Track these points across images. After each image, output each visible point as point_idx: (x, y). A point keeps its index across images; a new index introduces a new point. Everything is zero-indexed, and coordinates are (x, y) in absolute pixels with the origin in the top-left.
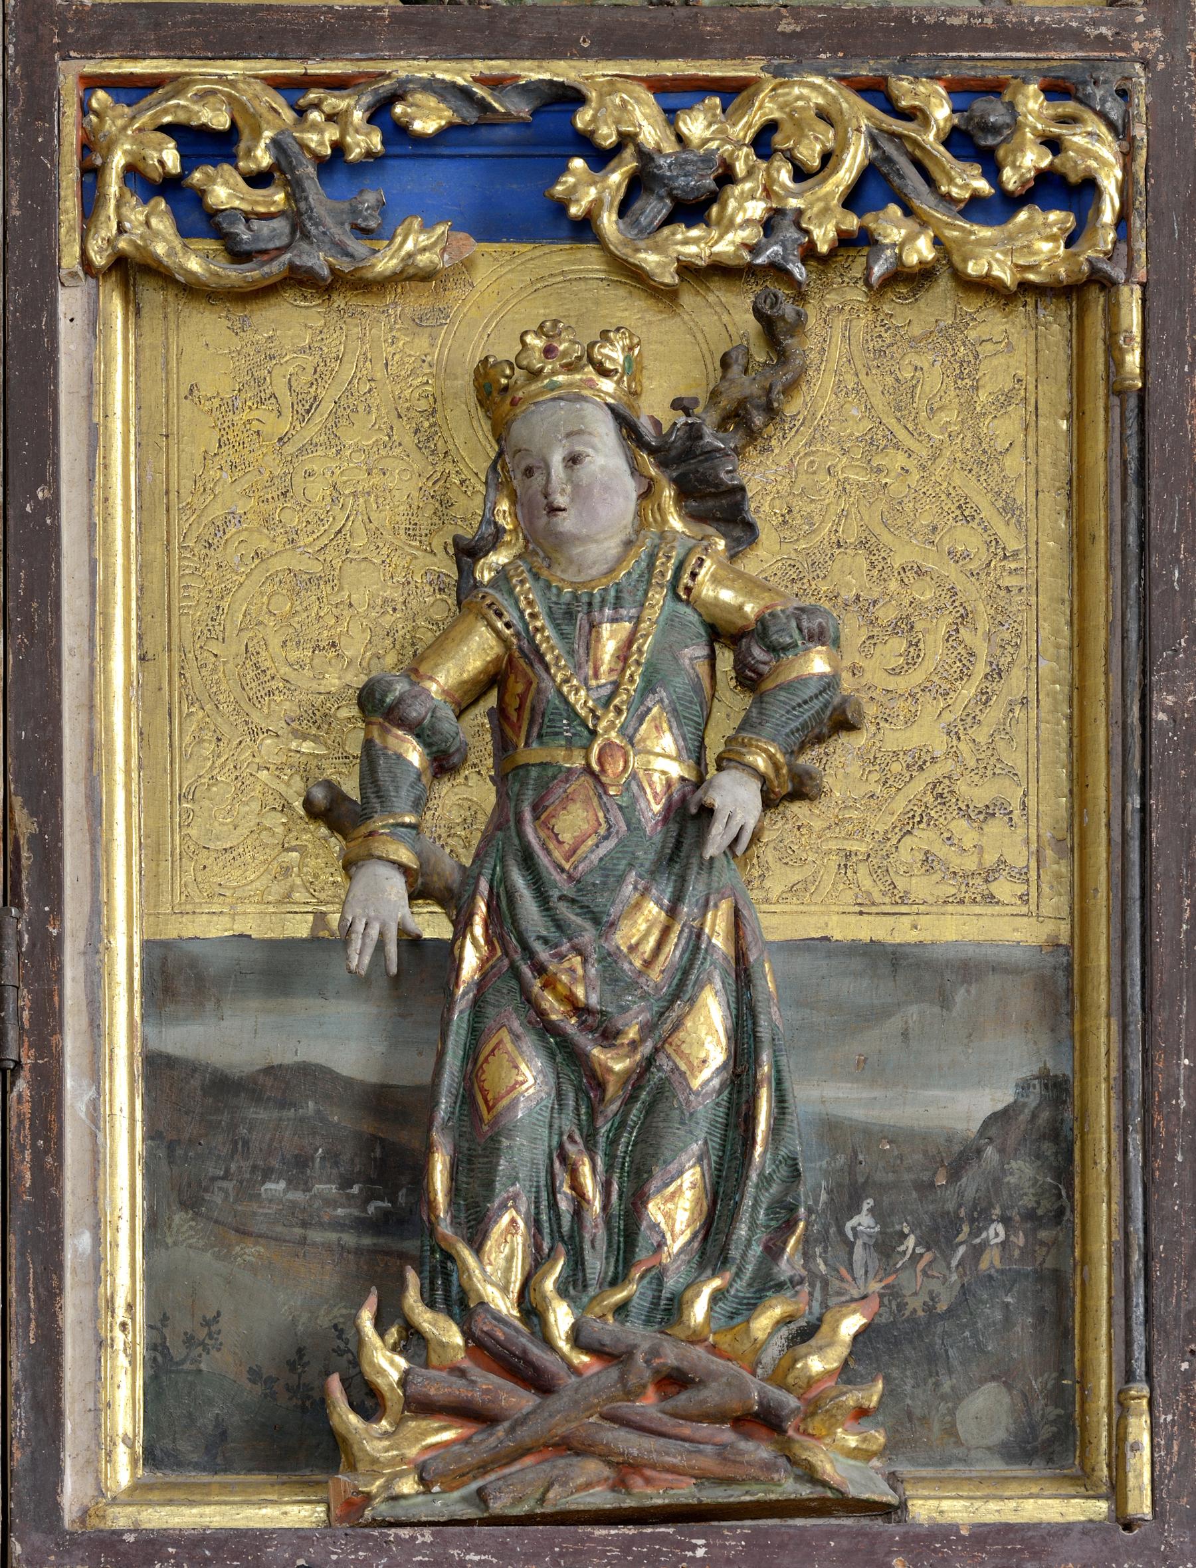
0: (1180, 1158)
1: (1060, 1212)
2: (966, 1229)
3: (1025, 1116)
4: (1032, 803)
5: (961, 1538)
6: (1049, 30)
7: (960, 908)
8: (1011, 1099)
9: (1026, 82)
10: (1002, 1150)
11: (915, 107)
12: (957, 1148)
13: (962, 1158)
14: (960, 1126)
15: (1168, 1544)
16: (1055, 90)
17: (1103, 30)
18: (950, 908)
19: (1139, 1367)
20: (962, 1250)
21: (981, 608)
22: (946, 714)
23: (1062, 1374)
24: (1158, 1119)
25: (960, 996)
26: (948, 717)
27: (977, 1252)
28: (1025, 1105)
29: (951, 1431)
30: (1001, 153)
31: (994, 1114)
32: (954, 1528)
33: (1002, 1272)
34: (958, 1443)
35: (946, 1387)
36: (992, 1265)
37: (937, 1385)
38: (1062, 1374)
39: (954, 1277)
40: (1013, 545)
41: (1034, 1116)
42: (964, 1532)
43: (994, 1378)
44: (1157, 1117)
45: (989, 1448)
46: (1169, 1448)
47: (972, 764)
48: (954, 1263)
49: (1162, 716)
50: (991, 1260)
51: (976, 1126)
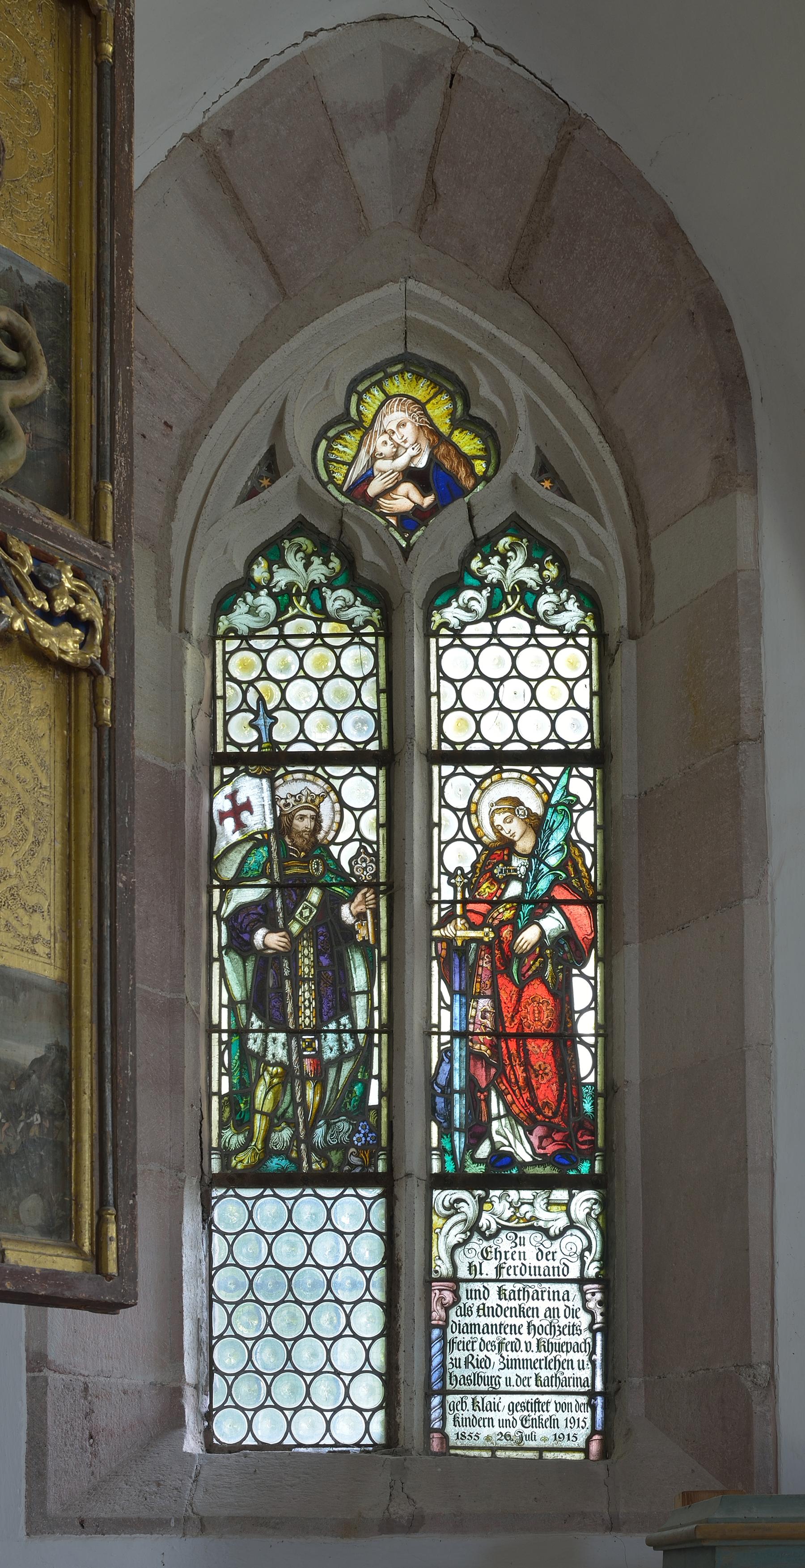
0: (128, 1100)
1: (64, 1114)
2: (24, 1114)
3: (49, 1063)
4: (52, 910)
5: (36, 1275)
6: (75, 543)
7: (21, 953)
8: (43, 1053)
9: (66, 563)
10: (39, 1078)
11: (18, 554)
12: (20, 1073)
13: (22, 1078)
14: (21, 1062)
15: (124, 1289)
16: (77, 575)
17: (98, 554)
18: (16, 951)
19: (111, 1198)
20: (22, 1124)
21: (31, 808)
22: (15, 856)
23: (64, 1195)
24: (120, 1080)
25: (21, 996)
26: (16, 857)
27: (29, 1126)
28: (49, 1057)
29: (17, 1216)
30: (55, 592)
31: (36, 1059)
32: (32, 1270)
33: (39, 1139)
34: (20, 1222)
35: (15, 1193)
36: (35, 1135)
37: (11, 1191)
38: (64, 1195)
39: (19, 1138)
40: (45, 783)
41: (53, 1064)
42: (37, 1272)
43: (36, 1192)
44: (119, 1078)
45: (33, 1227)
46: (125, 1241)
47: (27, 883)
48: (19, 1130)
49: (120, 885)
50: (34, 1132)
51: (28, 1063)
